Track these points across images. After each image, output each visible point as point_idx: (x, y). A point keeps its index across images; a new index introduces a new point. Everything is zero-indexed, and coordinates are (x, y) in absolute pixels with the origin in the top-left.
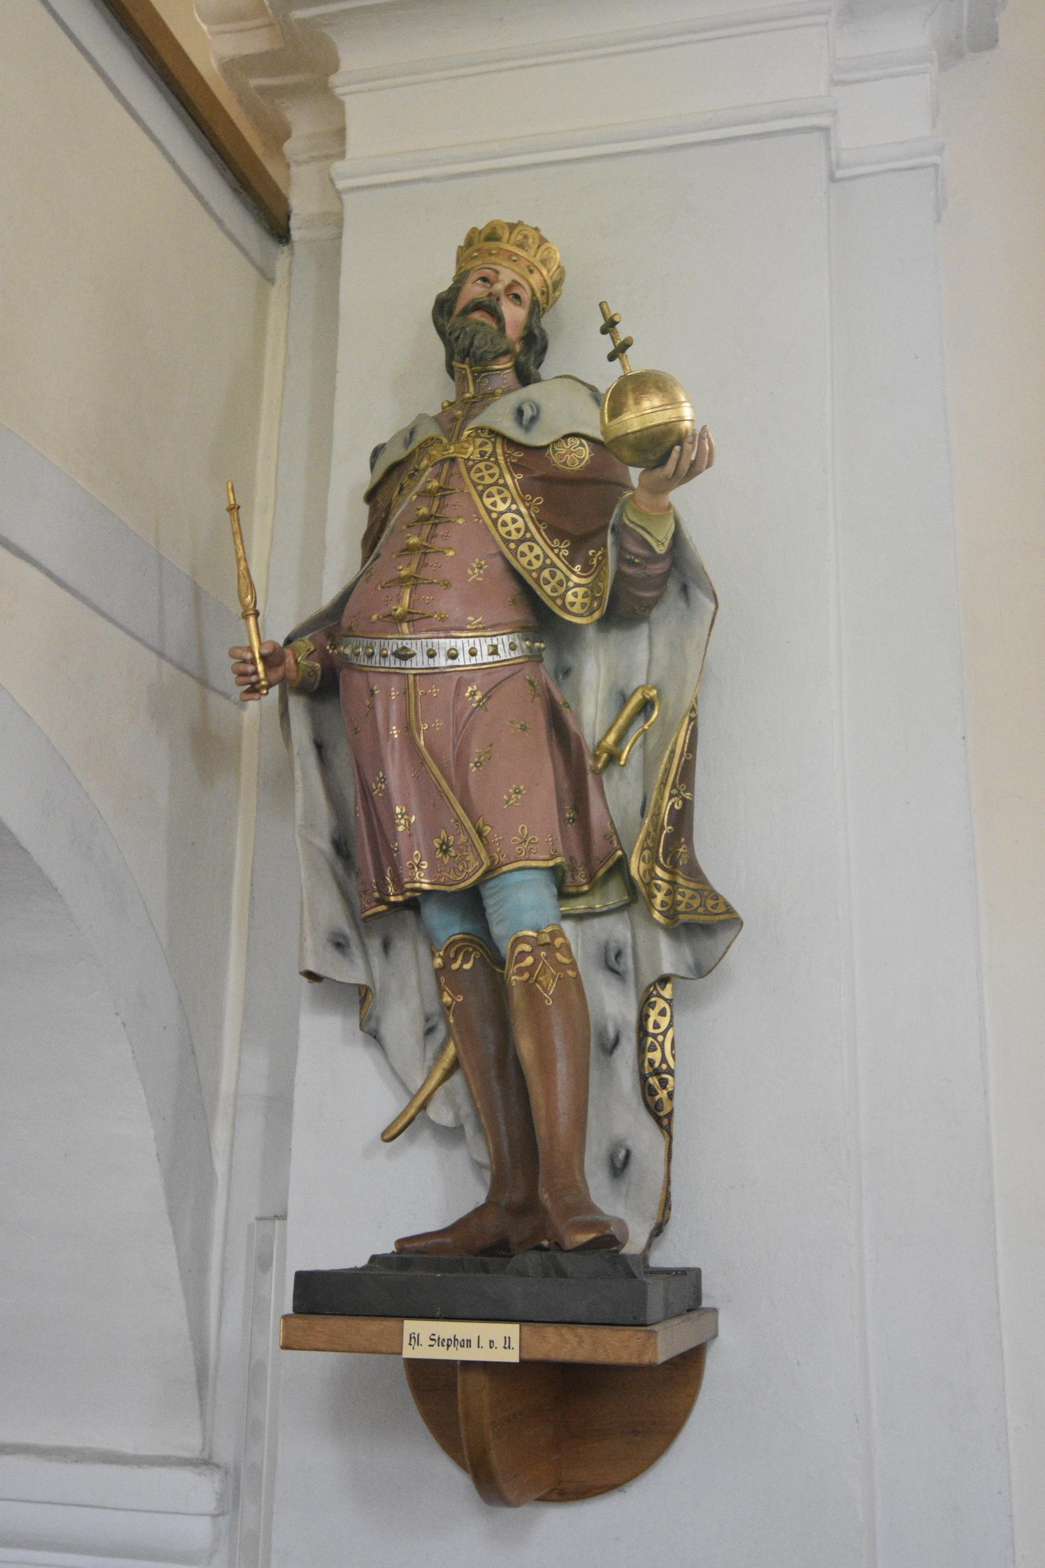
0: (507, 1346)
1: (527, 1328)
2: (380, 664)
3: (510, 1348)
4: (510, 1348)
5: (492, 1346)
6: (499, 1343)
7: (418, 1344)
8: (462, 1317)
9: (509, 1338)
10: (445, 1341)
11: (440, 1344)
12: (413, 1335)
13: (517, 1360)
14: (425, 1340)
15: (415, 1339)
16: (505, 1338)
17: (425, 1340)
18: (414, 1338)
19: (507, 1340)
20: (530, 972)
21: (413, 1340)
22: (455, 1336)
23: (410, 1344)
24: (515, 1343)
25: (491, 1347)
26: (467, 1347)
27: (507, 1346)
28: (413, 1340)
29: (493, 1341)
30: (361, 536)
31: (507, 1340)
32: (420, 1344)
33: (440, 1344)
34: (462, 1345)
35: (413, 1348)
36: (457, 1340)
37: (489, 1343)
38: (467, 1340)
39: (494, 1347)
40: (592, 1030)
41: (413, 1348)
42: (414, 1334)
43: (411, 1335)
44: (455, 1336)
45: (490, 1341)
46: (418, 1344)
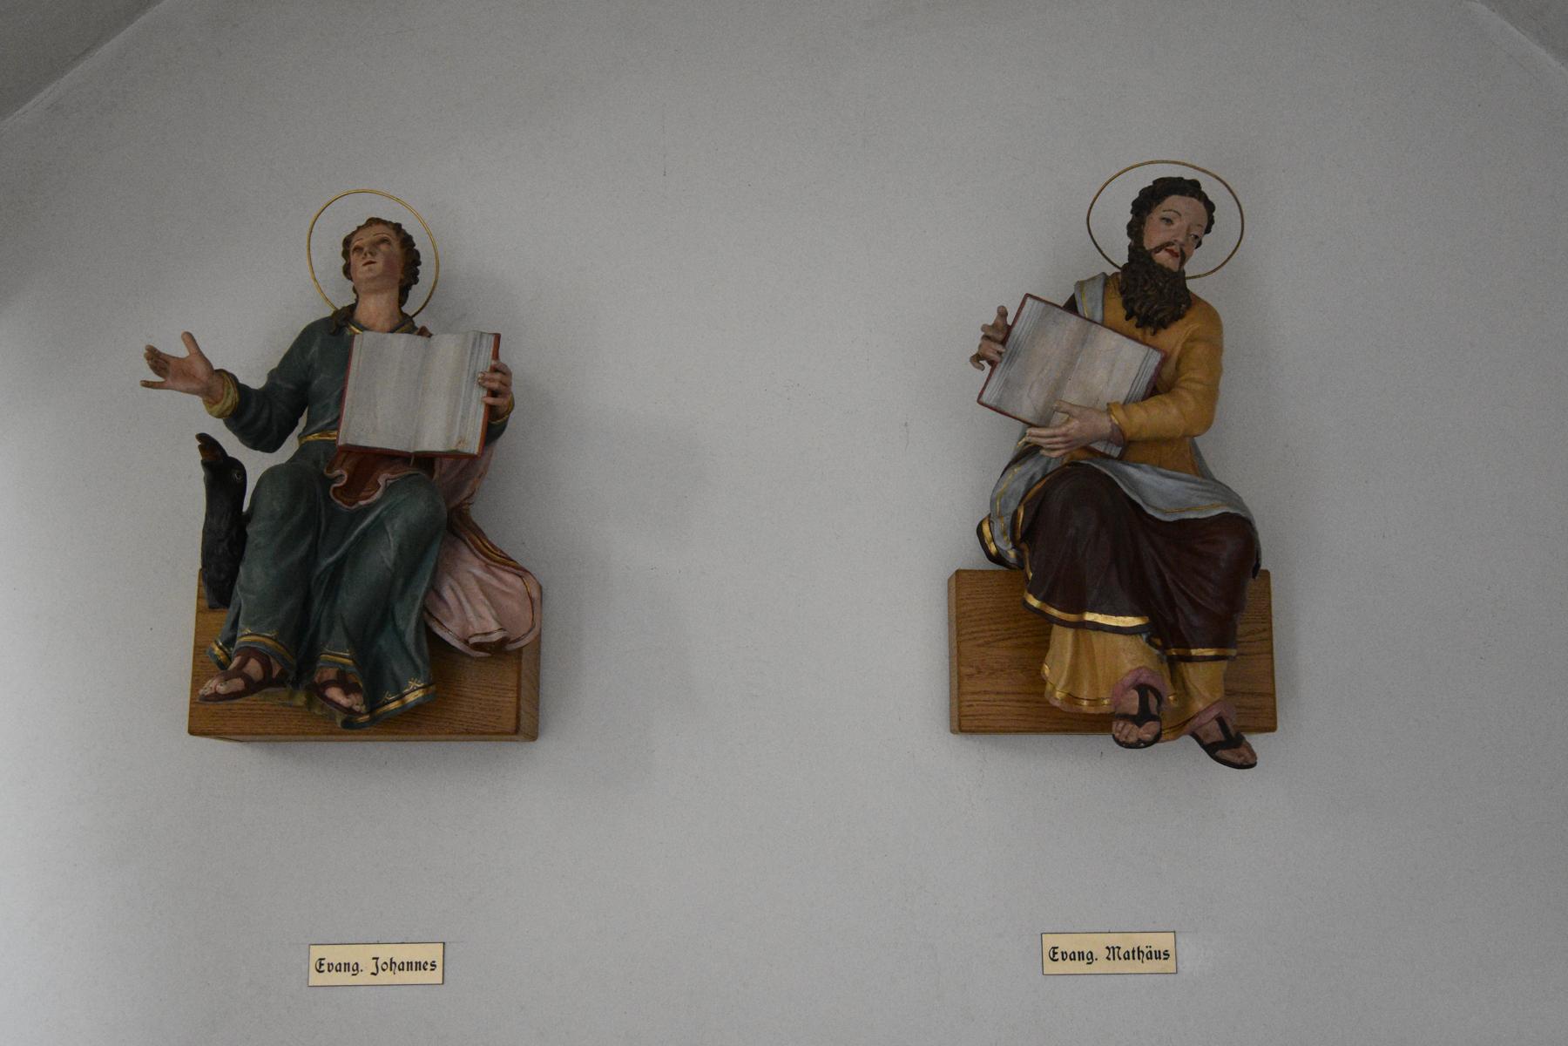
26: (1079, 959)
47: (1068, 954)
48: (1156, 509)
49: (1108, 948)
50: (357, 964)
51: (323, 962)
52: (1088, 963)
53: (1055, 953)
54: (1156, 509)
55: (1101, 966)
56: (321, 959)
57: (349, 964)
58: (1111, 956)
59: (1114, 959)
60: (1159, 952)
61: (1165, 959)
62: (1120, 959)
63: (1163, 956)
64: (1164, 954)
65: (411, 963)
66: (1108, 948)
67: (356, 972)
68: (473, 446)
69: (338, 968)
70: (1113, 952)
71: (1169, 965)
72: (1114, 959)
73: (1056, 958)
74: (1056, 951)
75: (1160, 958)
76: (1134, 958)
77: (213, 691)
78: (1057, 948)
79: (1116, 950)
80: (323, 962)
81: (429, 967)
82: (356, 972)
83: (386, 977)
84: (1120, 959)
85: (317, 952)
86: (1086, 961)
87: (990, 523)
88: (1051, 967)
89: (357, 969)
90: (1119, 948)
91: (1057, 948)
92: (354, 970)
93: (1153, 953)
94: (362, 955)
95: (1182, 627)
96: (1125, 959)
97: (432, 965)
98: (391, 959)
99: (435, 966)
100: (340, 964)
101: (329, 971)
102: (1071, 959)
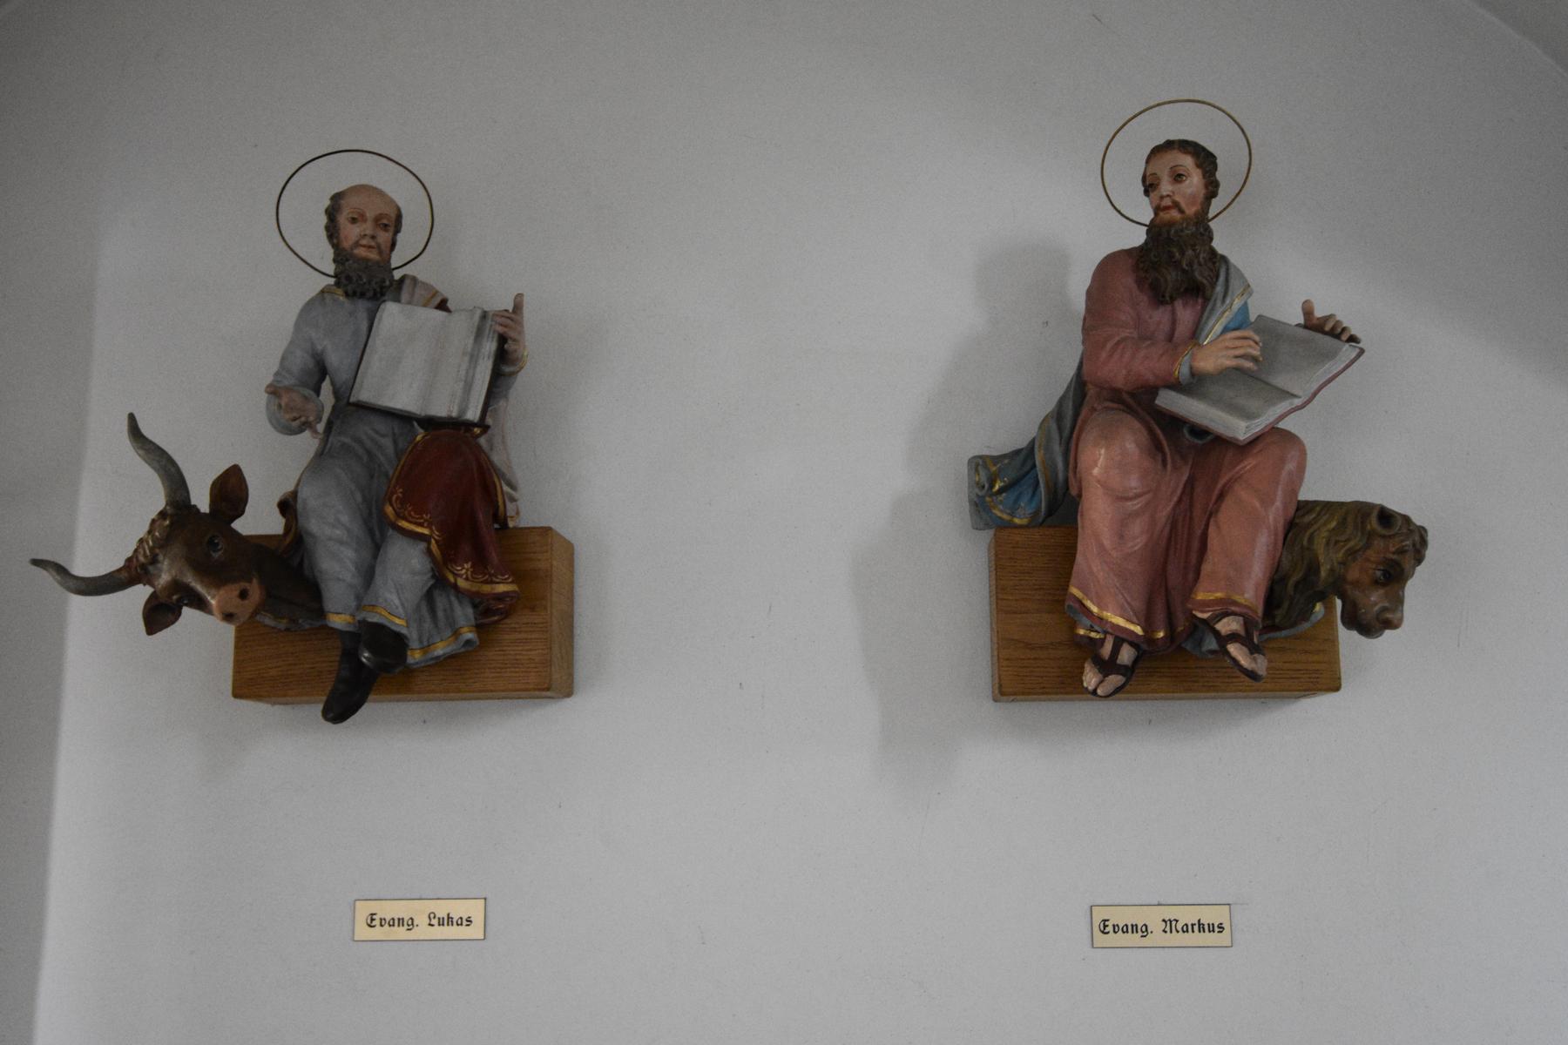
14: (421, 920)
19: (1211, 927)
26: (1133, 932)
44: (1199, 921)
47: (1120, 931)
48: (468, 387)
49: (1164, 920)
50: (412, 919)
51: (374, 917)
52: (1142, 936)
53: (1105, 926)
54: (468, 387)
55: (1156, 937)
56: (372, 914)
57: (403, 919)
58: (1168, 929)
59: (1171, 932)
60: (1213, 924)
61: (1219, 932)
62: (1178, 932)
63: (1217, 929)
64: (1219, 927)
65: (1210, 931)
66: (1164, 920)
67: (411, 927)
68: (473, 414)
69: (391, 923)
70: (1170, 925)
71: (1223, 938)
72: (1171, 932)
73: (374, 923)
74: (1107, 923)
75: (1213, 931)
76: (1193, 931)
77: (474, 629)
78: (1108, 920)
79: (1174, 923)
80: (374, 917)
81: (465, 923)
82: (411, 927)
83: (378, 933)
84: (1178, 932)
85: (373, 907)
86: (406, 927)
87: (1343, 523)
88: (1100, 939)
89: (412, 924)
90: (1177, 921)
91: (1108, 920)
92: (408, 925)
93: (1139, 930)
94: (418, 911)
95: (1301, 575)
96: (1184, 932)
97: (467, 921)
98: (448, 915)
99: (1223, 928)
100: (393, 919)
101: (381, 925)
102: (1124, 932)
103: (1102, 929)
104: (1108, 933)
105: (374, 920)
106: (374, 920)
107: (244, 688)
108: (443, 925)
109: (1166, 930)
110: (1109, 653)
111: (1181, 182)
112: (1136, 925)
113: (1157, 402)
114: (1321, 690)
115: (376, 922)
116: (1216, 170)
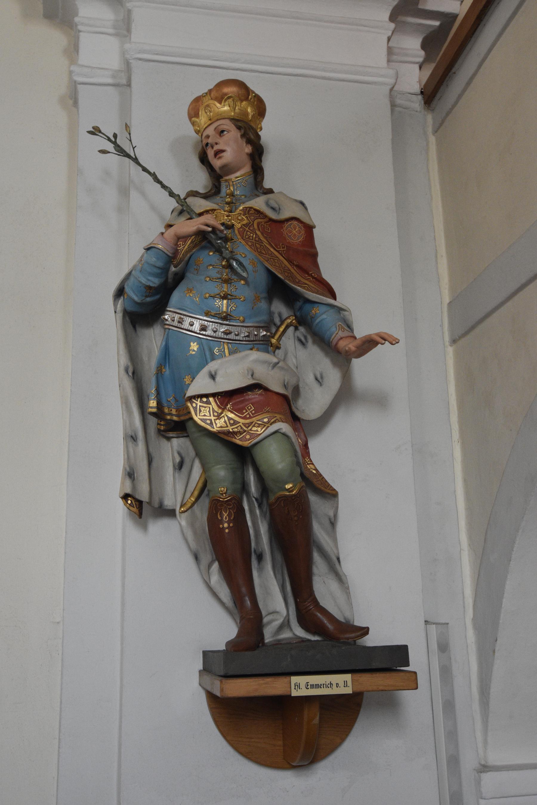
0: (345, 685)
1: (357, 676)
2: (195, 295)
3: (347, 687)
4: (347, 687)
5: (338, 686)
6: (341, 684)
7: (299, 689)
8: (430, 685)
9: (346, 681)
10: (321, 685)
11: (327, 687)
12: (296, 684)
13: (351, 692)
14: (303, 686)
15: (297, 686)
16: (344, 681)
17: (303, 686)
18: (297, 685)
19: (346, 682)
20: (231, 259)
21: (296, 686)
22: (330, 682)
23: (295, 689)
24: (350, 683)
25: (337, 687)
26: (316, 688)
27: (346, 685)
28: (296, 686)
29: (338, 684)
30: (370, 630)
31: (346, 682)
32: (300, 688)
33: (327, 687)
34: (337, 685)
35: (297, 691)
36: (332, 684)
37: (336, 685)
38: (315, 685)
39: (339, 687)
40: (307, 292)
41: (297, 691)
42: (297, 683)
43: (295, 684)
44: (330, 682)
45: (336, 684)
46: (299, 689)
56: (307, 683)
78: (308, 683)
80: (308, 684)
91: (308, 683)
103: (306, 686)
104: (308, 689)
105: (308, 685)
106: (308, 685)
107: (206, 654)
108: (315, 685)
109: (345, 686)
110: (308, 494)
111: (217, 143)
112: (318, 685)
113: (313, 229)
114: (342, 384)
115: (309, 687)
116: (169, 194)
